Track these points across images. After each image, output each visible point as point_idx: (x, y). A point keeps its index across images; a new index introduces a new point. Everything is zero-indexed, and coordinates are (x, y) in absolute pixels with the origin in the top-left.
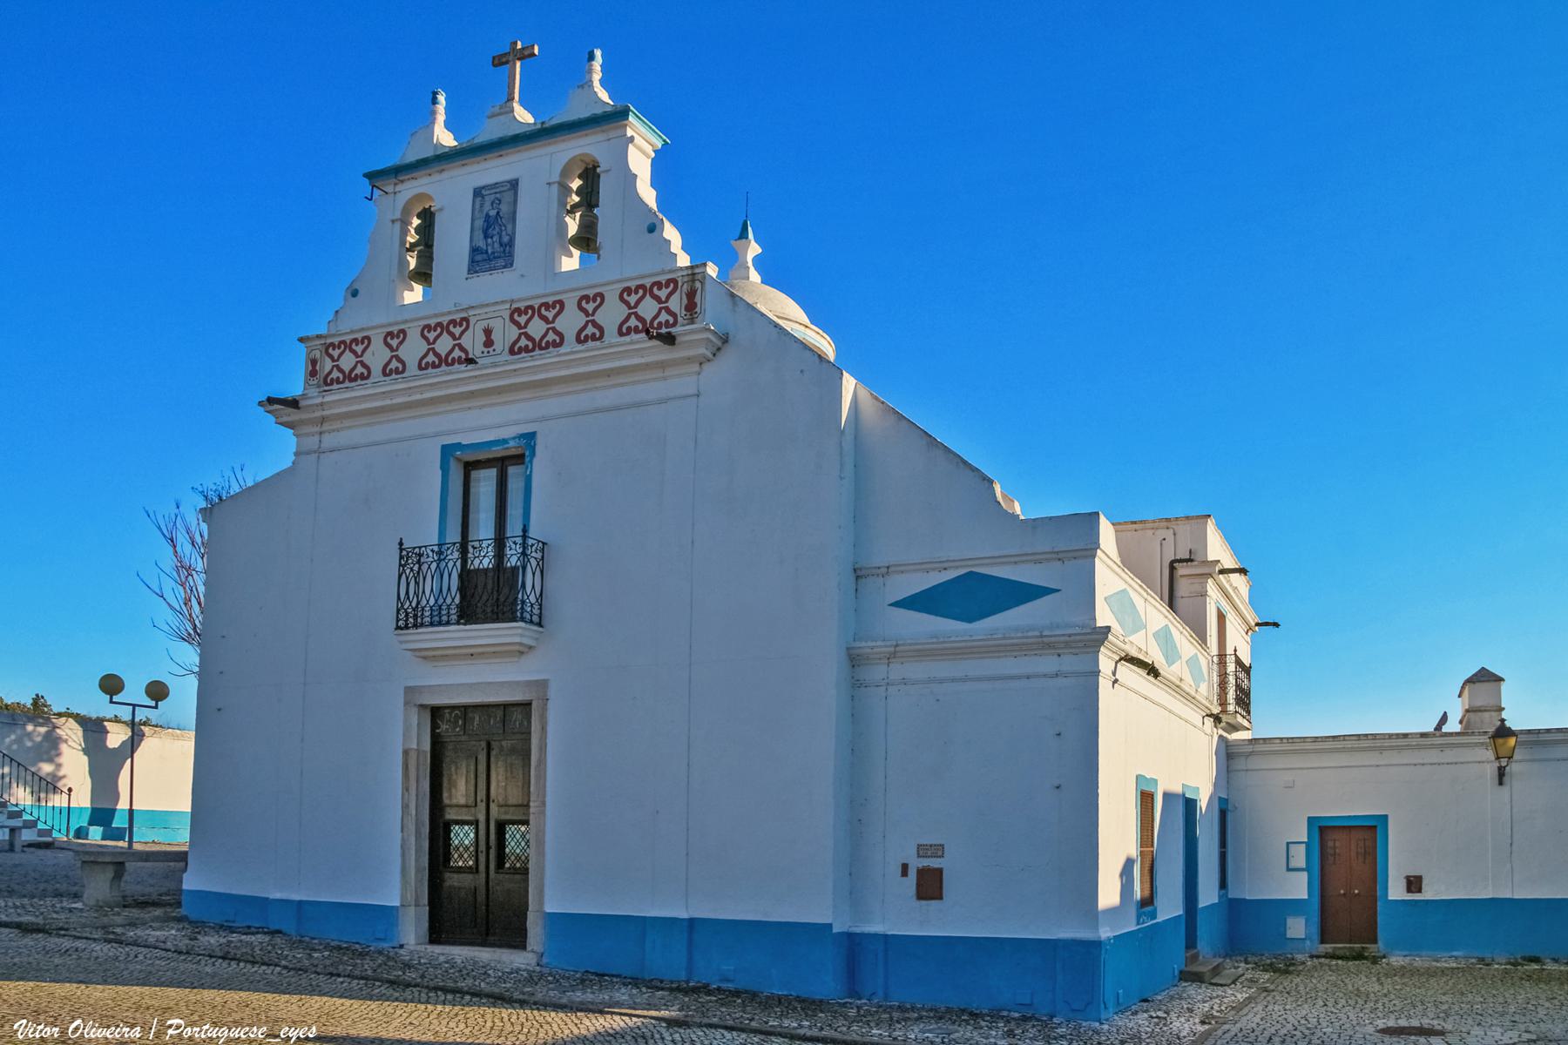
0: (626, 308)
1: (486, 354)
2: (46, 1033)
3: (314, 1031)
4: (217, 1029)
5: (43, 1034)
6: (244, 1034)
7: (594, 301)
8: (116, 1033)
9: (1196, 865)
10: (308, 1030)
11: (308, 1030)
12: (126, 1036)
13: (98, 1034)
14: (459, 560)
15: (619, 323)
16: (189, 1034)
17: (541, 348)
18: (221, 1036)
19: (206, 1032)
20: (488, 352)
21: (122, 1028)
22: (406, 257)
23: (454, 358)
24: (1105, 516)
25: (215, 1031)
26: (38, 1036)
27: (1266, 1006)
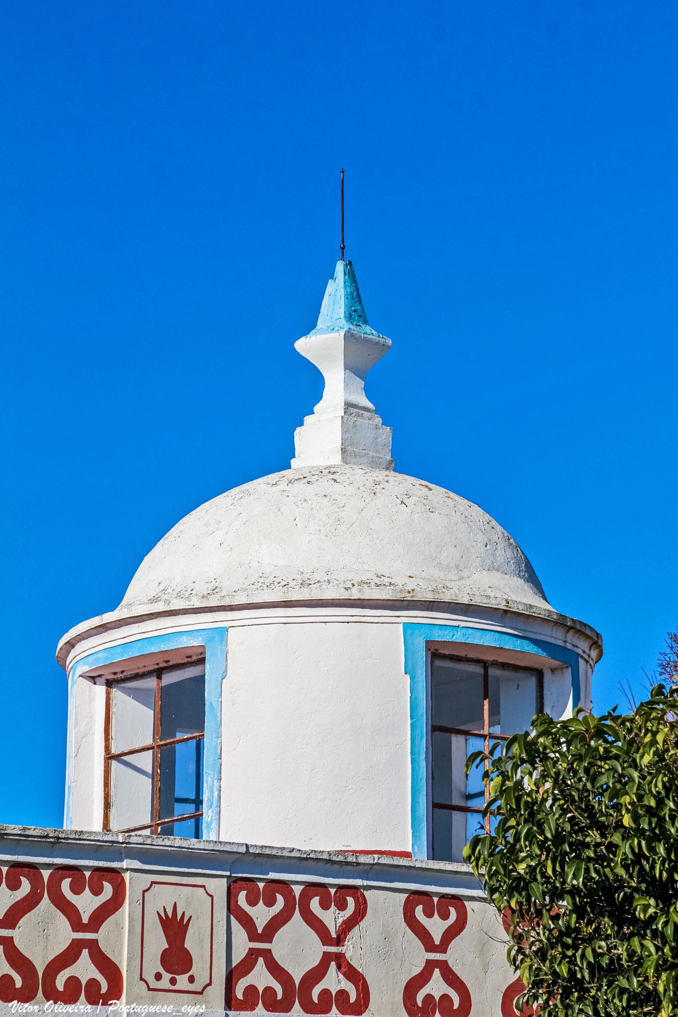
0: (276, 956)
1: (165, 983)
2: (30, 1009)
3: (204, 1008)
4: (141, 1007)
5: (28, 1010)
6: (72, 1010)
7: (73, 982)
8: (75, 1009)
9: (227, 893)
10: (162, 1007)
11: (200, 1008)
12: (82, 1011)
13: (63, 1010)
14: (602, 952)
15: (364, 923)
16: (31, 1010)
17: (52, 995)
18: (143, 1011)
19: (133, 1009)
20: (173, 981)
21: (79, 1006)
22: (585, 987)
23: (325, 993)
24: (560, 717)
25: (139, 1008)
26: (24, 1011)
27: (194, 909)
